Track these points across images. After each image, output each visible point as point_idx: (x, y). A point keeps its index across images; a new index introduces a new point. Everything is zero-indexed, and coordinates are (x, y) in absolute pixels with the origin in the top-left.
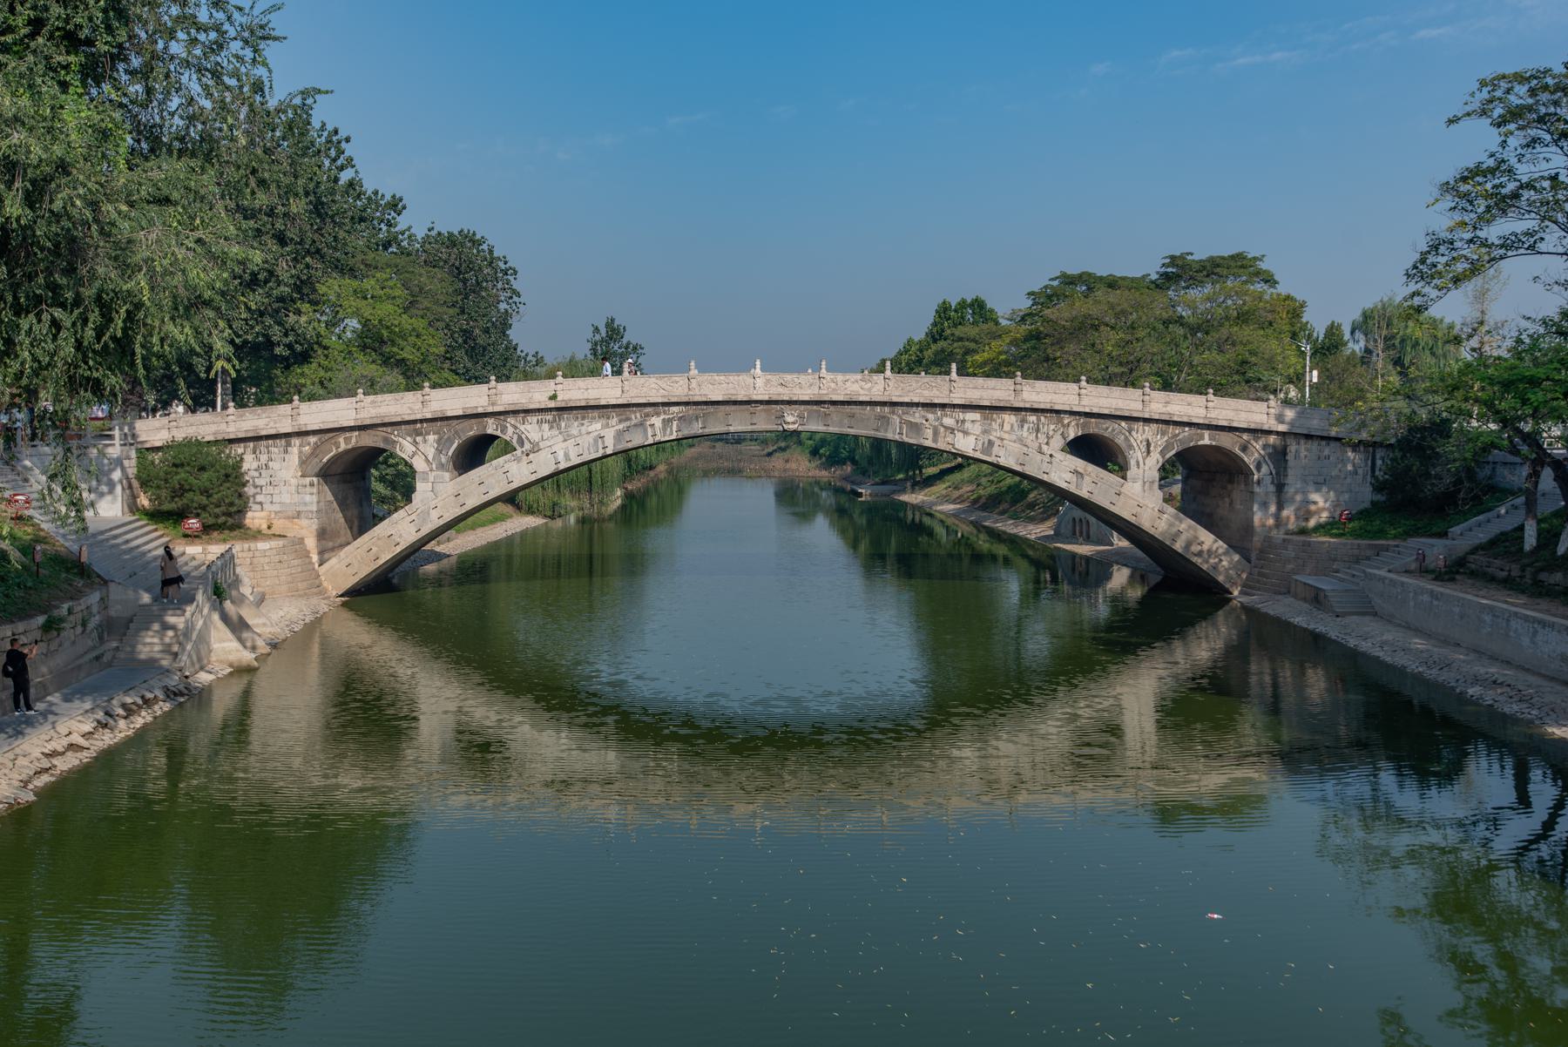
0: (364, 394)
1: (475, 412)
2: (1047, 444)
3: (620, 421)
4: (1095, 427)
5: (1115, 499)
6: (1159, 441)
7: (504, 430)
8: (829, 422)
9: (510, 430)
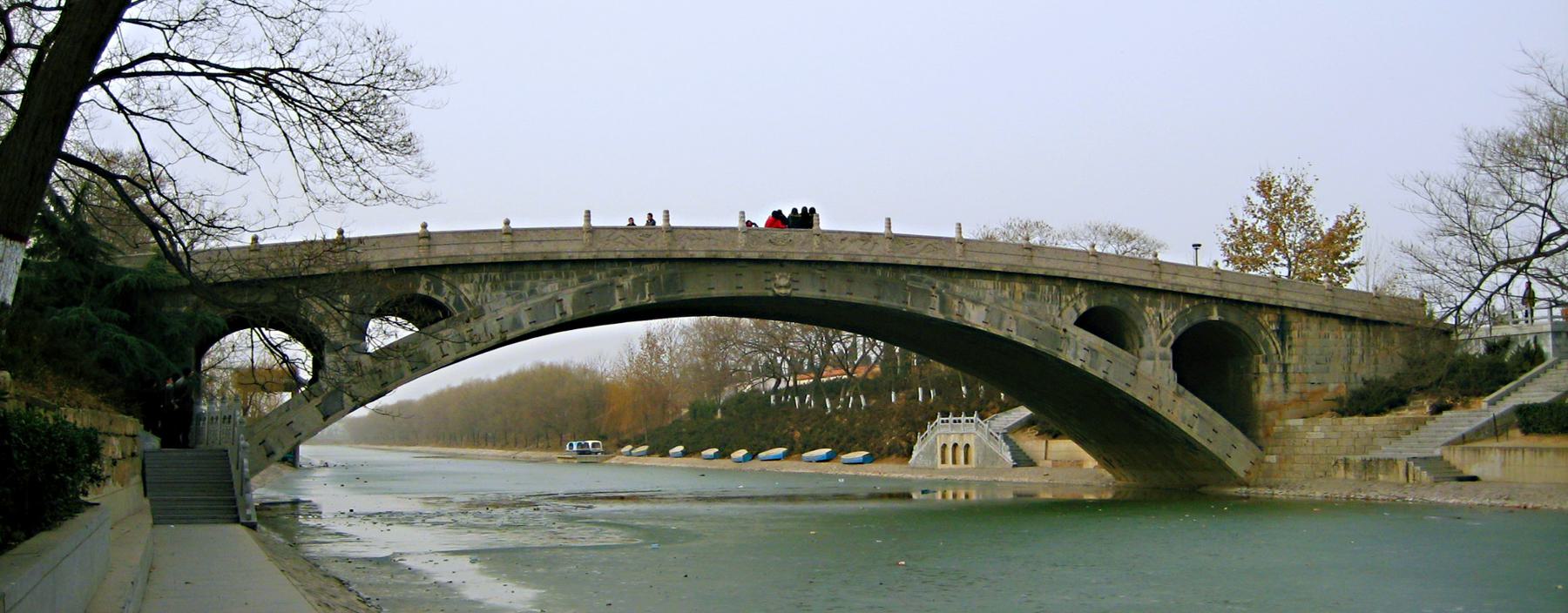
0: (19, 409)
1: (405, 265)
2: (1060, 316)
3: (582, 281)
4: (1110, 300)
5: (1155, 394)
6: (1169, 316)
7: (438, 290)
8: (826, 287)
9: (446, 289)
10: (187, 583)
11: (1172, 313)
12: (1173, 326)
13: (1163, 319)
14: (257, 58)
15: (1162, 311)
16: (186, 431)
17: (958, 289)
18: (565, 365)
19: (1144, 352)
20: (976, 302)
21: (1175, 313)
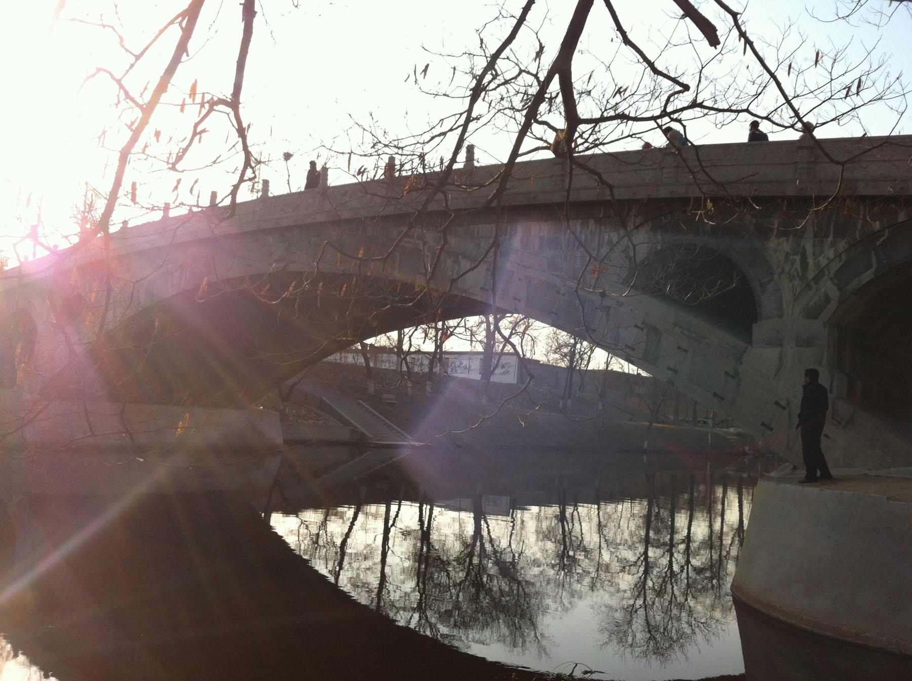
10: (425, 26)
11: (834, 244)
12: (837, 274)
13: (810, 260)
19: (760, 330)
21: (842, 245)
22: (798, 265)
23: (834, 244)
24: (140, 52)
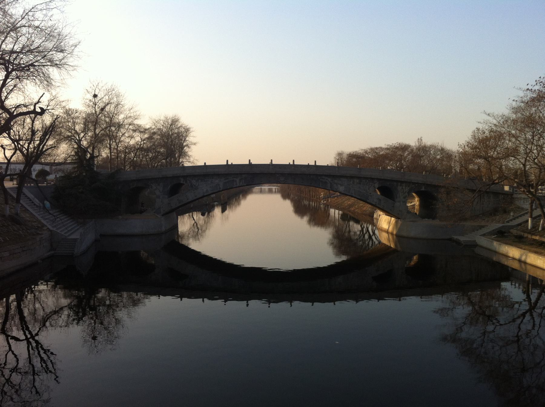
2: (369, 189)
9: (188, 182)
12: (408, 192)
13: (404, 190)
14: (29, 37)
15: (404, 188)
16: (209, 212)
17: (336, 181)
18: (246, 197)
20: (341, 185)
22: (402, 191)
23: (407, 188)
24: (22, 339)
